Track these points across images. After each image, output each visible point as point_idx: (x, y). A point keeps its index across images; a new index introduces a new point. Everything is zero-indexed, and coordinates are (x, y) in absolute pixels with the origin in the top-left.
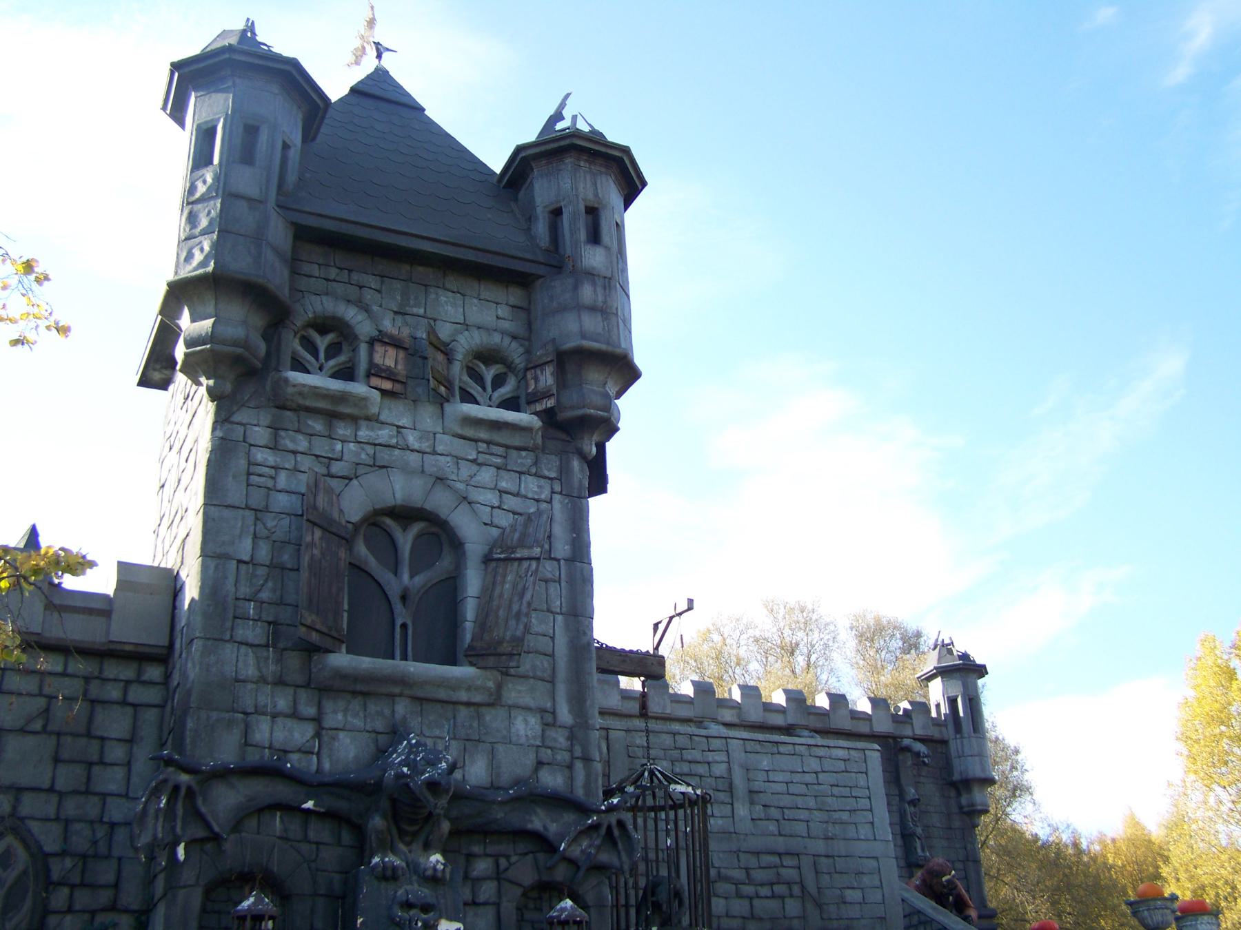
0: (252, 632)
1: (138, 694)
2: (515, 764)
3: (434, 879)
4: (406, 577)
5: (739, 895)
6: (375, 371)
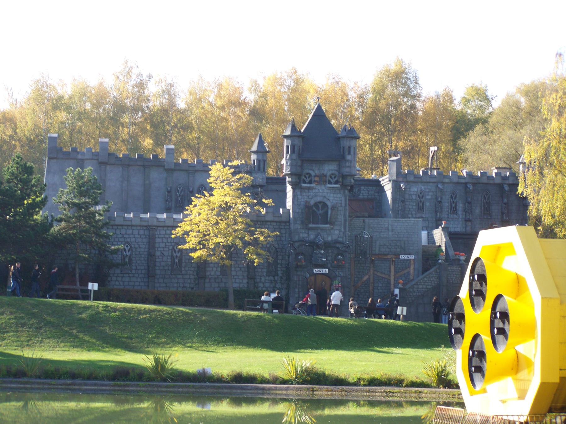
0: (299, 222)
1: (286, 227)
2: (335, 237)
3: (322, 254)
4: (320, 211)
5: (388, 248)
6: (315, 181)
